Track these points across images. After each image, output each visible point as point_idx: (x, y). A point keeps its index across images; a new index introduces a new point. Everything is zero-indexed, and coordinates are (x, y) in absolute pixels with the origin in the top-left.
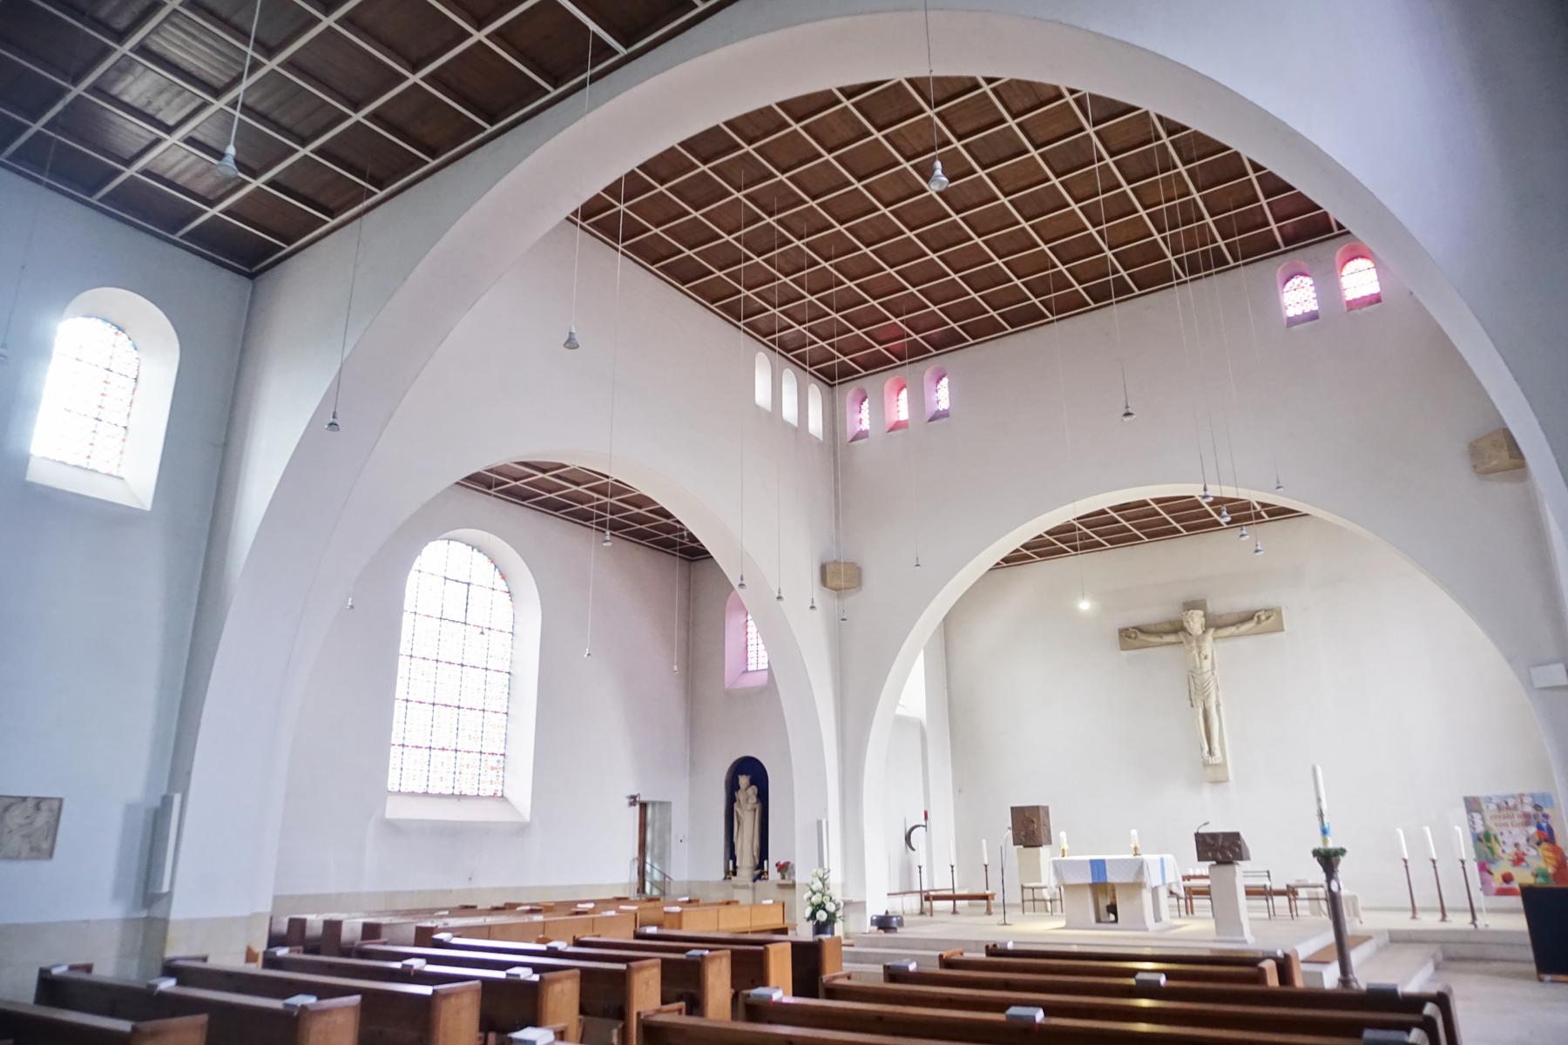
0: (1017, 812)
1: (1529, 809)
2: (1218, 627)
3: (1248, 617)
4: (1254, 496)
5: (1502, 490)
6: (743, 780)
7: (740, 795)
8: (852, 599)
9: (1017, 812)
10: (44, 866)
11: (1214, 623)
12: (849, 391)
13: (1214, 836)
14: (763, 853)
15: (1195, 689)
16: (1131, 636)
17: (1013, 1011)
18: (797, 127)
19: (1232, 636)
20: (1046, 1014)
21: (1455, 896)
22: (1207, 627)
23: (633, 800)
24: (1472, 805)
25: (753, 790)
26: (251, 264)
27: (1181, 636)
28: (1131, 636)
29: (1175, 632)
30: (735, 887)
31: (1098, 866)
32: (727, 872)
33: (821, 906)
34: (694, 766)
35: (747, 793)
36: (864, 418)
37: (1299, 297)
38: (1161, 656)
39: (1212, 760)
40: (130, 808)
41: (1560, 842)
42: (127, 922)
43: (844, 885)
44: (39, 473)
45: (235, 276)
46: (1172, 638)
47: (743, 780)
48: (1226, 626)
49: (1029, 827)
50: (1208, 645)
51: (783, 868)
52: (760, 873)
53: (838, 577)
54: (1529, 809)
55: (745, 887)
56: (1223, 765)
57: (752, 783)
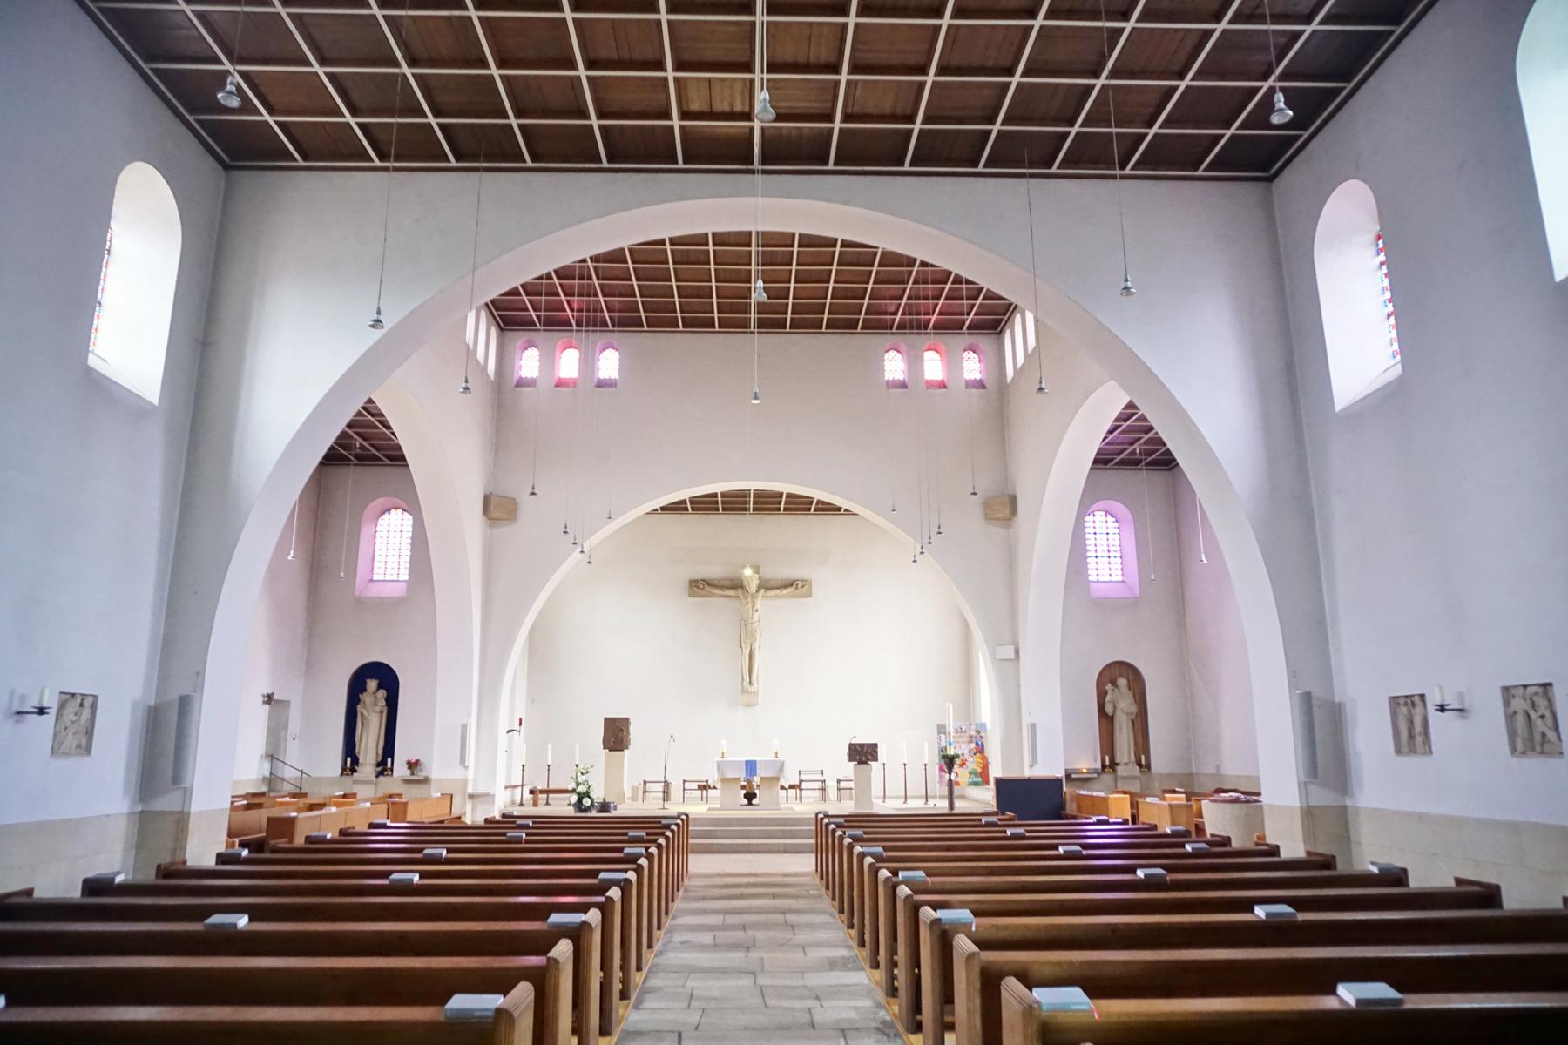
0: (609, 722)
1: (973, 733)
2: (767, 589)
3: (791, 584)
4: (818, 495)
5: (997, 531)
6: (372, 684)
7: (366, 698)
8: (504, 531)
9: (609, 722)
10: (85, 762)
11: (765, 586)
12: (518, 337)
13: (862, 745)
14: (389, 749)
15: (745, 633)
16: (699, 586)
17: (217, 919)
18: (495, 72)
19: (777, 596)
20: (251, 920)
21: (916, 787)
22: (759, 588)
23: (269, 699)
24: (942, 729)
25: (382, 693)
26: (232, 159)
27: (740, 592)
28: (699, 586)
29: (734, 587)
30: (355, 782)
31: (751, 766)
32: (344, 768)
33: (587, 794)
34: (311, 666)
35: (373, 699)
36: (529, 363)
37: (894, 366)
38: (719, 606)
39: (751, 689)
40: (135, 704)
41: (987, 753)
42: (131, 814)
43: (475, 780)
44: (92, 361)
45: (215, 164)
46: (732, 593)
47: (372, 684)
48: (772, 588)
49: (616, 735)
50: (760, 603)
51: (413, 765)
52: (383, 766)
53: (497, 508)
54: (973, 733)
55: (369, 782)
56: (757, 693)
57: (380, 687)
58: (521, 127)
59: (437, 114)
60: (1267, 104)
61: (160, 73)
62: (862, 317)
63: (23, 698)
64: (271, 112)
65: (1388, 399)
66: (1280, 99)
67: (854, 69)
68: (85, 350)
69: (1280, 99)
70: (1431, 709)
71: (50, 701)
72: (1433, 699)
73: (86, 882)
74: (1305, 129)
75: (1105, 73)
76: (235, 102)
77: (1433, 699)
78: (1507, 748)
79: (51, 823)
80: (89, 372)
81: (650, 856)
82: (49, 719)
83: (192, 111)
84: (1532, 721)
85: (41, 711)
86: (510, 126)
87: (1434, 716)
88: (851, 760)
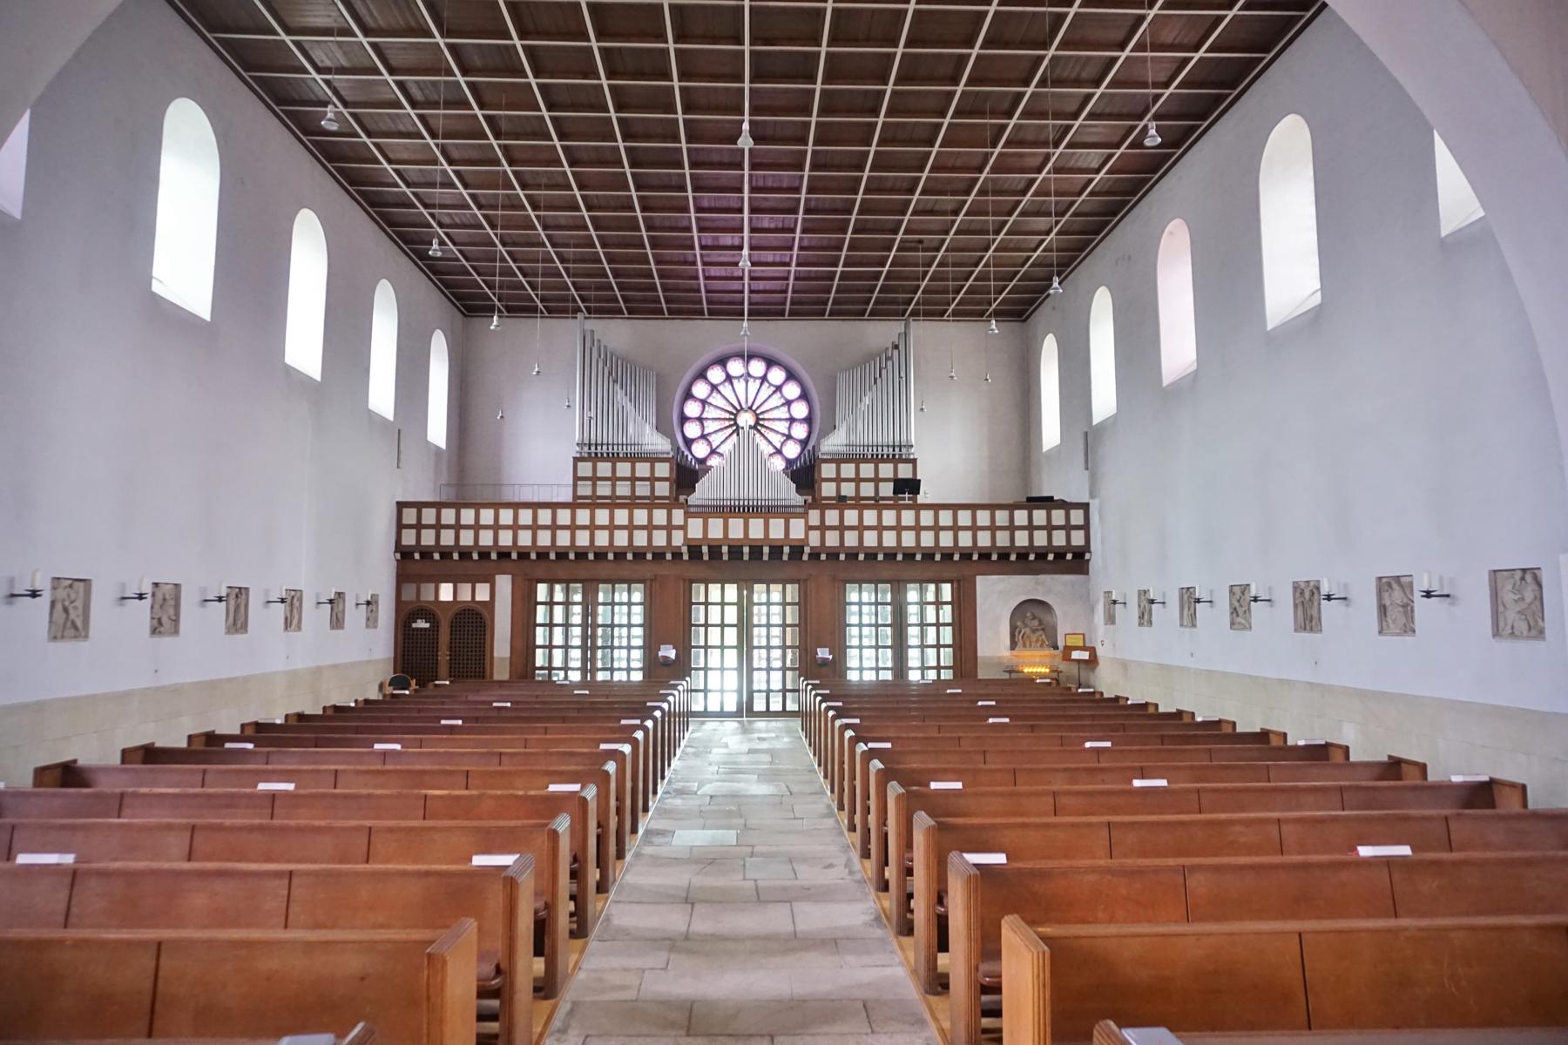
44: (289, 360)
58: (541, 87)
59: (464, 74)
60: (1145, 129)
61: (315, 143)
62: (859, 197)
63: (204, 590)
64: (369, 135)
65: (1312, 322)
66: (1153, 132)
67: (798, 265)
68: (149, 278)
69: (1153, 132)
70: (1417, 596)
71: (43, 584)
72: (1325, 590)
73: (124, 752)
74: (1268, 52)
75: (988, 169)
76: (334, 127)
77: (1325, 590)
78: (1489, 631)
79: (76, 699)
80: (157, 300)
81: (646, 729)
82: (147, 603)
83: (371, 205)
84: (1520, 601)
85: (34, 594)
86: (529, 84)
87: (1419, 603)
88: (1390, 757)
